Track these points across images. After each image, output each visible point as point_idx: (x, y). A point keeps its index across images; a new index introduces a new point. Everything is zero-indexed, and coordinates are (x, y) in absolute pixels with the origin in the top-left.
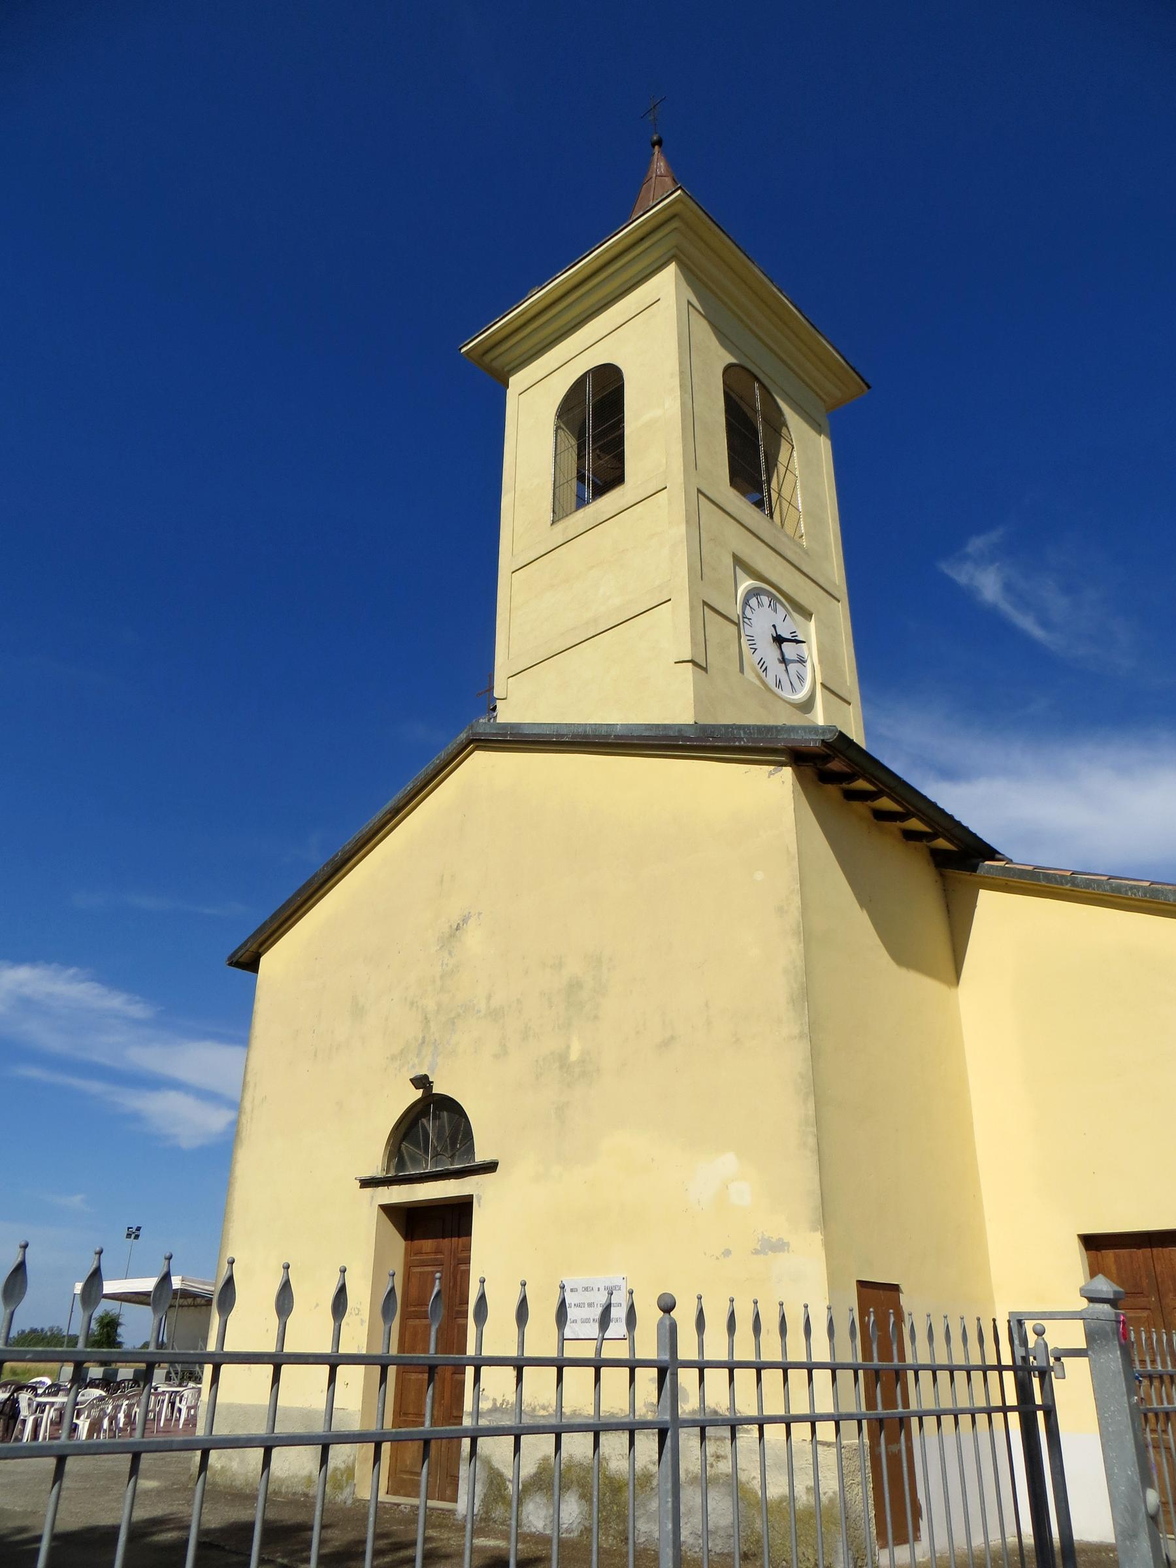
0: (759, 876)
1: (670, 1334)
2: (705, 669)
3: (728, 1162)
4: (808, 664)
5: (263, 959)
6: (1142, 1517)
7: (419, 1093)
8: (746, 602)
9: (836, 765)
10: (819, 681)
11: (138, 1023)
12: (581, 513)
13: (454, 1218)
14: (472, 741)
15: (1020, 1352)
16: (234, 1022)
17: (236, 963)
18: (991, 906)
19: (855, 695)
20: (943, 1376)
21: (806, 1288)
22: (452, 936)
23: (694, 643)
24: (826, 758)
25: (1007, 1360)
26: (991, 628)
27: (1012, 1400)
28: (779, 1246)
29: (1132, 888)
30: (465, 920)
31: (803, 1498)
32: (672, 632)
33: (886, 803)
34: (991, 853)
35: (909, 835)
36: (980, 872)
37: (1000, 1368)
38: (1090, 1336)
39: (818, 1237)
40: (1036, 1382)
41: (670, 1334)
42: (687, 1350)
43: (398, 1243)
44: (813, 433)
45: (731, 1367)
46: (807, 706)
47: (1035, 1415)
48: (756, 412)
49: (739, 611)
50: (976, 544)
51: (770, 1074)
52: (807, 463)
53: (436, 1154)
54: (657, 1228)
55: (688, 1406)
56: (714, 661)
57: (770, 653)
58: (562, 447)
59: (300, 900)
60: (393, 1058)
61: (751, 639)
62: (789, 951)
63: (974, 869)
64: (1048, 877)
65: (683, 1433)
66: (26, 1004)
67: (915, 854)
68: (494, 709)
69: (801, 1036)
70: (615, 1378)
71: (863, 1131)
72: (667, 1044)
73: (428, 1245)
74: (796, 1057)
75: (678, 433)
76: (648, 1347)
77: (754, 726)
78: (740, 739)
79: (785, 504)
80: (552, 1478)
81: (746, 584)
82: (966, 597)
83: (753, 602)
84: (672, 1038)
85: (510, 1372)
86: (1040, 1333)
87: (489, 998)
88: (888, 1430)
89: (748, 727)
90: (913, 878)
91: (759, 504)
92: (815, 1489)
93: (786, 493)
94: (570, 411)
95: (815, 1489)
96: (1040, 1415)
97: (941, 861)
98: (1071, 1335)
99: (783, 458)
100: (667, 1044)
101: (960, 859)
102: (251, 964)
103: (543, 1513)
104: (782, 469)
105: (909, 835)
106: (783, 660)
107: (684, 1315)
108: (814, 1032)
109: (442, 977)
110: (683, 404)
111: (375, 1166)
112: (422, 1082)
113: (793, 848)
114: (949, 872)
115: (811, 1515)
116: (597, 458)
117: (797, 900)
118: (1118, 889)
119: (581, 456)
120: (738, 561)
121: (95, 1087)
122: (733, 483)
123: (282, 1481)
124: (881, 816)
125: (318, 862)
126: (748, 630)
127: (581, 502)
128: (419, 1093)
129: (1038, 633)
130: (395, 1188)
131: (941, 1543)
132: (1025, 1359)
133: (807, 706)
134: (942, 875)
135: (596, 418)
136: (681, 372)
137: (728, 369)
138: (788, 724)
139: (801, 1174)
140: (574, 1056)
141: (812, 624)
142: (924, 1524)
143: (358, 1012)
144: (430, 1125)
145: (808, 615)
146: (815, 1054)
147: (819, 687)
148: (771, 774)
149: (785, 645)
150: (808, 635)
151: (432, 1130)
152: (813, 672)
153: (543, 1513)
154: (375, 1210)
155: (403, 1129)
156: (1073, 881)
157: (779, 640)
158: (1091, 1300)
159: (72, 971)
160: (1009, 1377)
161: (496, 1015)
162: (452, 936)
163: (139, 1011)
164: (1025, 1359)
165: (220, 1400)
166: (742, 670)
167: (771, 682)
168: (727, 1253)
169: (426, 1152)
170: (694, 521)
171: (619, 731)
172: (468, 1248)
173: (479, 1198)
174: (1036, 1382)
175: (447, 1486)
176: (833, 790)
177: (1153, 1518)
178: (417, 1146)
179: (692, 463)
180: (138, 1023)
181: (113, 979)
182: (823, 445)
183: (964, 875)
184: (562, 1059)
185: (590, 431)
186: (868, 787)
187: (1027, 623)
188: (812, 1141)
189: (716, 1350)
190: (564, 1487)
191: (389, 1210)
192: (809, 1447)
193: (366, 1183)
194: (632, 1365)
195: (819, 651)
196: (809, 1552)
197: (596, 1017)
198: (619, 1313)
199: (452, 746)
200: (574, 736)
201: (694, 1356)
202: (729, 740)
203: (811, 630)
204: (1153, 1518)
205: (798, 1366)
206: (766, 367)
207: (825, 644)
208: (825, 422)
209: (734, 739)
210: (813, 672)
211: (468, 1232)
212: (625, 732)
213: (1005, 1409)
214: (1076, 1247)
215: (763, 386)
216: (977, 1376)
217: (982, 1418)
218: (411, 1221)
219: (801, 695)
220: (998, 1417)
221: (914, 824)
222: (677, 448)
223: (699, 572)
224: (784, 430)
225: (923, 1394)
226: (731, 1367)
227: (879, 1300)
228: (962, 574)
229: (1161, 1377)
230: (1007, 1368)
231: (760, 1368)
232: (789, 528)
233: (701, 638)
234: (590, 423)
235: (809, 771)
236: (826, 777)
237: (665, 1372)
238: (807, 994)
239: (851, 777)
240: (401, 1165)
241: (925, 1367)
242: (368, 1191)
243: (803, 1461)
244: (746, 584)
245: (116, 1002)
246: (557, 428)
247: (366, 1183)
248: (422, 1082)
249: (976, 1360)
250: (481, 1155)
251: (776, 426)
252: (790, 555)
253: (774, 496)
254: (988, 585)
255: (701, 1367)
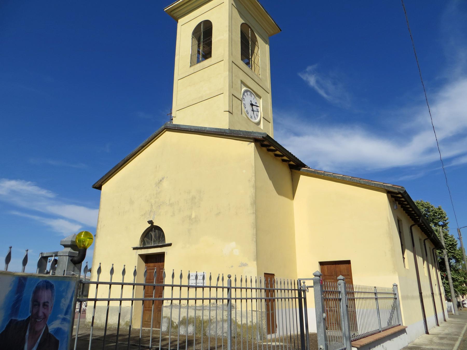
0: (244, 171)
1: (230, 282)
2: (232, 114)
3: (233, 244)
4: (260, 113)
5: (103, 187)
6: (322, 319)
7: (150, 225)
8: (244, 94)
9: (266, 143)
10: (262, 119)
11: (50, 199)
12: (199, 65)
13: (160, 258)
14: (165, 128)
15: (299, 287)
16: (95, 203)
17: (95, 187)
18: (304, 180)
19: (271, 121)
20: (283, 291)
21: (252, 273)
22: (159, 183)
23: (229, 106)
24: (263, 141)
25: (296, 288)
26: (311, 94)
27: (297, 296)
28: (245, 265)
29: (338, 176)
30: (163, 179)
31: (249, 324)
32: (223, 102)
33: (278, 153)
34: (304, 166)
35: (284, 161)
36: (301, 170)
37: (295, 290)
38: (314, 283)
39: (255, 262)
40: (302, 293)
41: (230, 282)
42: (233, 285)
43: (144, 264)
44: (264, 44)
45: (241, 288)
46: (258, 123)
47: (302, 299)
48: (249, 37)
49: (242, 97)
50: (309, 68)
51: (246, 221)
52: (262, 52)
53: (154, 241)
54: (212, 259)
55: (233, 296)
56: (235, 111)
57: (249, 108)
58: (193, 44)
59: (114, 170)
60: (142, 215)
61: (244, 104)
62: (251, 191)
63: (299, 170)
64: (318, 173)
65: (232, 300)
66: (13, 192)
67: (284, 165)
68: (172, 120)
69: (253, 213)
70: (220, 290)
71: (267, 235)
72: (218, 214)
73: (152, 265)
74: (251, 219)
75: (228, 45)
76: (226, 285)
77: (245, 131)
78: (241, 134)
79: (256, 65)
80: (186, 321)
81: (244, 89)
82: (305, 84)
83: (246, 94)
84: (220, 213)
85: (202, 289)
86: (304, 283)
87: (170, 200)
88: (270, 301)
89: (243, 131)
90: (284, 171)
91: (248, 64)
92: (252, 322)
93: (256, 62)
94: (196, 33)
95: (252, 322)
96: (303, 299)
97: (291, 167)
98: (311, 283)
99: (256, 51)
100: (218, 214)
101: (296, 166)
102: (100, 188)
103: (183, 330)
104: (255, 55)
105: (284, 161)
106: (253, 110)
107: (233, 279)
108: (256, 213)
109: (156, 194)
110: (229, 36)
111: (137, 244)
112: (151, 222)
113: (253, 165)
114: (293, 170)
115: (251, 327)
116: (204, 47)
117: (254, 178)
118: (335, 177)
119: (199, 47)
120: (242, 82)
121: (37, 218)
122: (242, 59)
123: (112, 325)
124: (276, 155)
125: (119, 161)
126: (244, 102)
127: (198, 62)
128: (150, 225)
129: (325, 95)
130: (143, 250)
131: (281, 334)
132: (301, 288)
133: (258, 123)
134: (291, 171)
135: (204, 33)
136: (229, 26)
137: (242, 25)
138: (254, 131)
139: (252, 247)
140: (193, 216)
141: (261, 100)
142: (277, 329)
143: (132, 202)
144: (153, 234)
145: (260, 97)
146: (256, 218)
147: (262, 118)
148: (248, 144)
149: (253, 107)
150: (260, 104)
151: (153, 234)
152: (261, 114)
153: (183, 330)
154: (137, 256)
155: (145, 234)
156: (324, 174)
157: (252, 105)
158: (315, 276)
159: (29, 183)
160: (297, 292)
161: (171, 205)
162: (159, 183)
163: (51, 195)
164: (301, 288)
165: (96, 305)
166: (242, 114)
167: (249, 117)
168: (232, 266)
169: (152, 240)
170: (231, 71)
171: (208, 129)
172: (164, 266)
173: (167, 253)
174: (302, 293)
175: (158, 323)
176: (264, 149)
177: (324, 319)
178: (149, 239)
179: (231, 54)
180: (50, 199)
181: (42, 186)
182: (267, 47)
183: (297, 171)
184: (190, 217)
185: (202, 40)
186: (274, 148)
187: (322, 93)
188: (255, 239)
189: (238, 285)
190: (189, 323)
191: (140, 255)
192: (251, 312)
193: (134, 249)
194: (223, 288)
195: (263, 108)
196: (250, 336)
197: (199, 206)
198: (221, 279)
199: (160, 130)
200: (195, 130)
201: (234, 286)
202: (238, 134)
203: (260, 103)
204: (324, 319)
205: (244, 299)
206: (252, 23)
207: (265, 104)
208: (268, 41)
209: (239, 134)
210: (261, 114)
211: (163, 261)
212: (209, 130)
213: (295, 298)
214: (318, 264)
215: (251, 30)
216: (290, 291)
217: (290, 300)
218: (147, 259)
219: (257, 120)
220: (294, 300)
221: (285, 158)
222: (227, 49)
223: (231, 86)
224: (257, 43)
225: (278, 294)
226: (241, 288)
227: (269, 277)
228: (304, 77)
229: (327, 292)
230: (296, 290)
231: (246, 289)
232: (256, 73)
233: (231, 105)
234: (202, 37)
235: (259, 144)
236: (263, 145)
237: (229, 289)
238: (255, 202)
239: (270, 146)
240: (144, 244)
241: (279, 289)
242: (135, 251)
243: (249, 315)
244: (244, 89)
245: (43, 192)
246: (193, 37)
247: (134, 249)
248: (151, 222)
249: (290, 288)
250: (167, 242)
251: (254, 41)
252: (256, 80)
253: (253, 62)
254: (312, 80)
255: (236, 288)
